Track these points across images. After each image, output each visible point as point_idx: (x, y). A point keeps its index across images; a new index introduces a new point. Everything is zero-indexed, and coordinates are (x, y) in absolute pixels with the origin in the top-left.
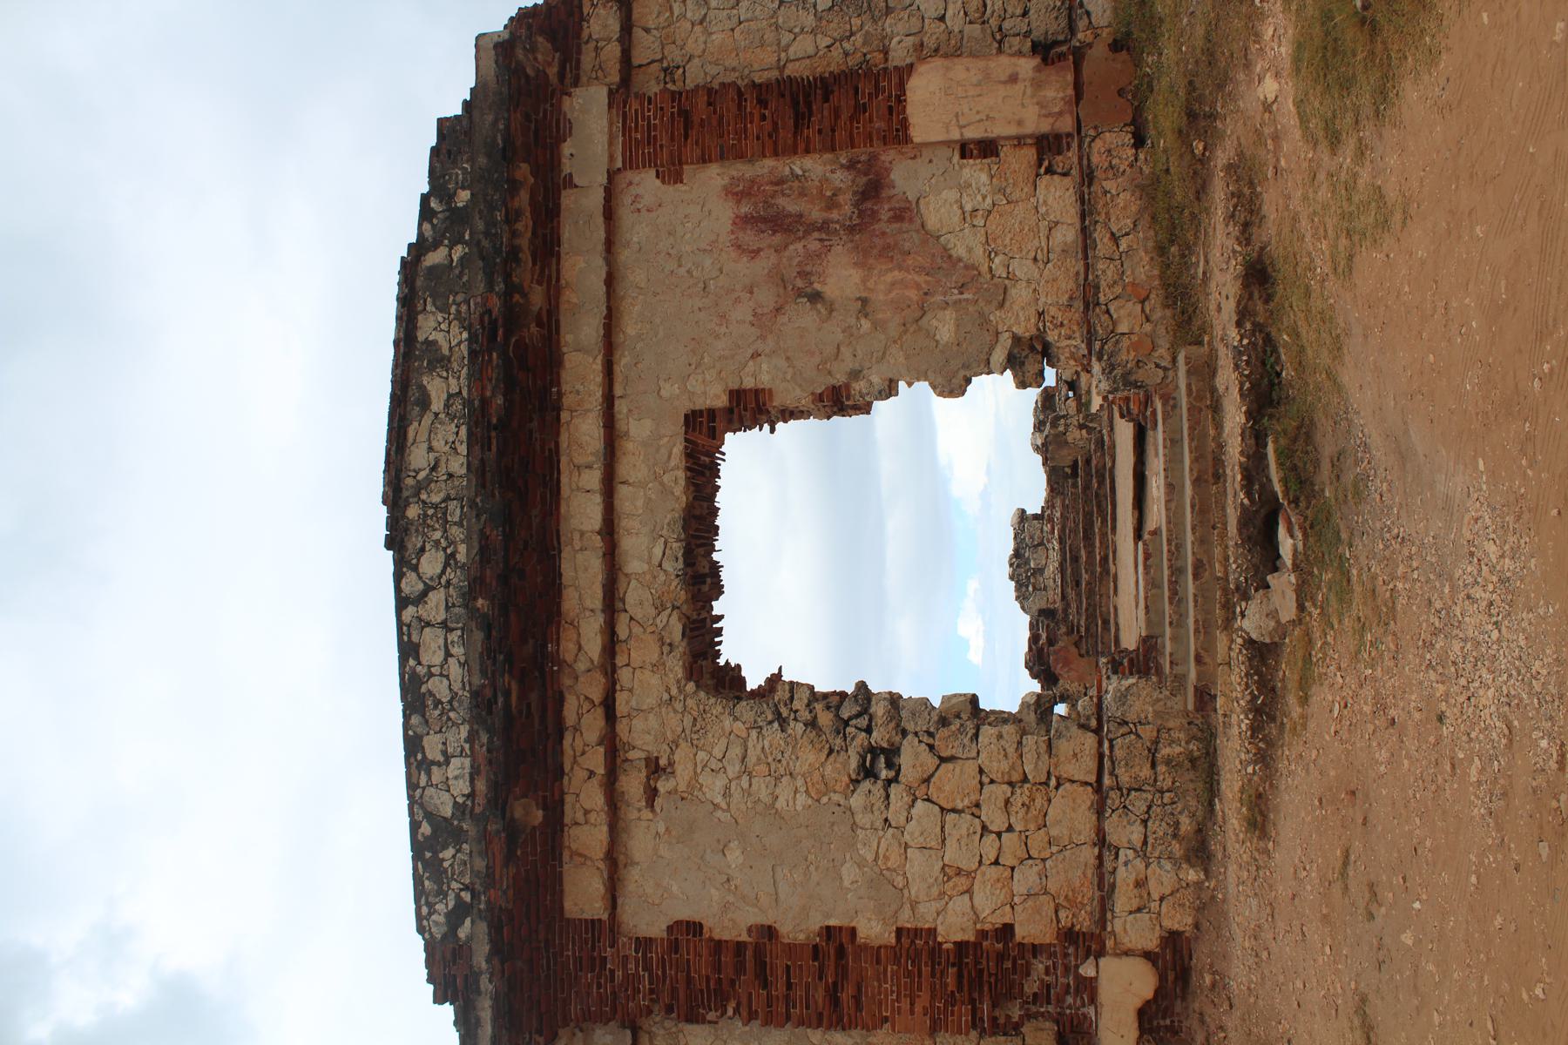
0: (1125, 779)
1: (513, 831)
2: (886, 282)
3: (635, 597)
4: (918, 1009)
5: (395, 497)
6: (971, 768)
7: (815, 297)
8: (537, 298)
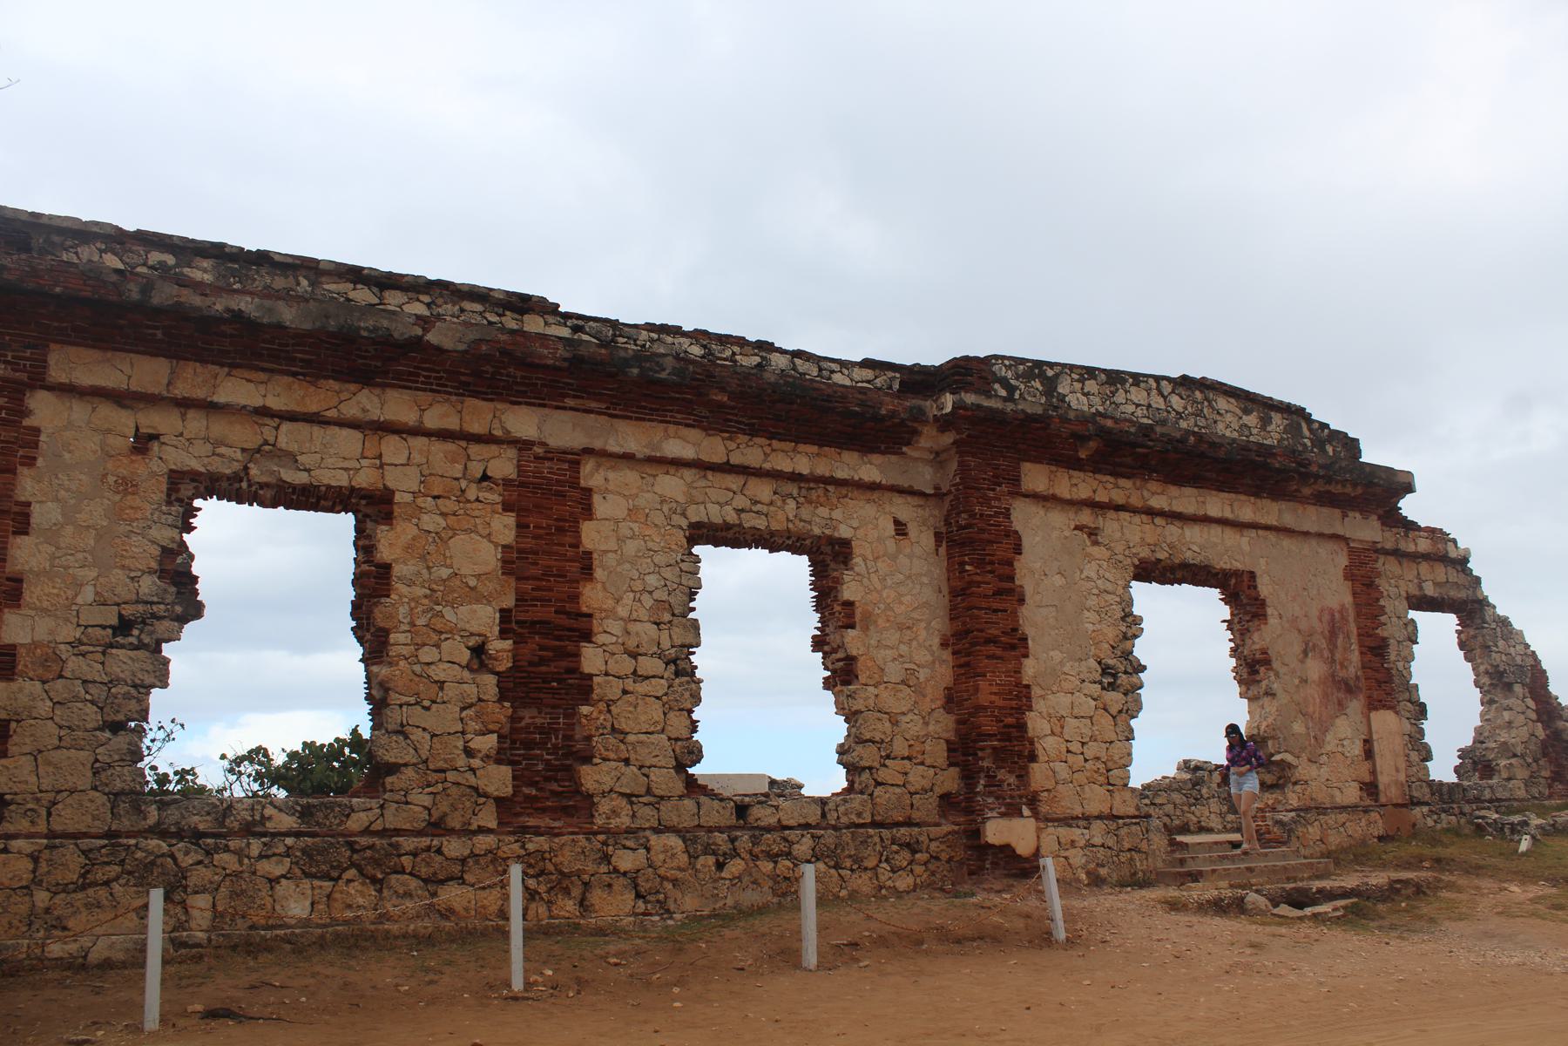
1: (1082, 439)
2: (1313, 693)
3: (1173, 531)
4: (993, 698)
5: (1205, 385)
6: (1113, 737)
7: (1305, 653)
8: (1306, 491)
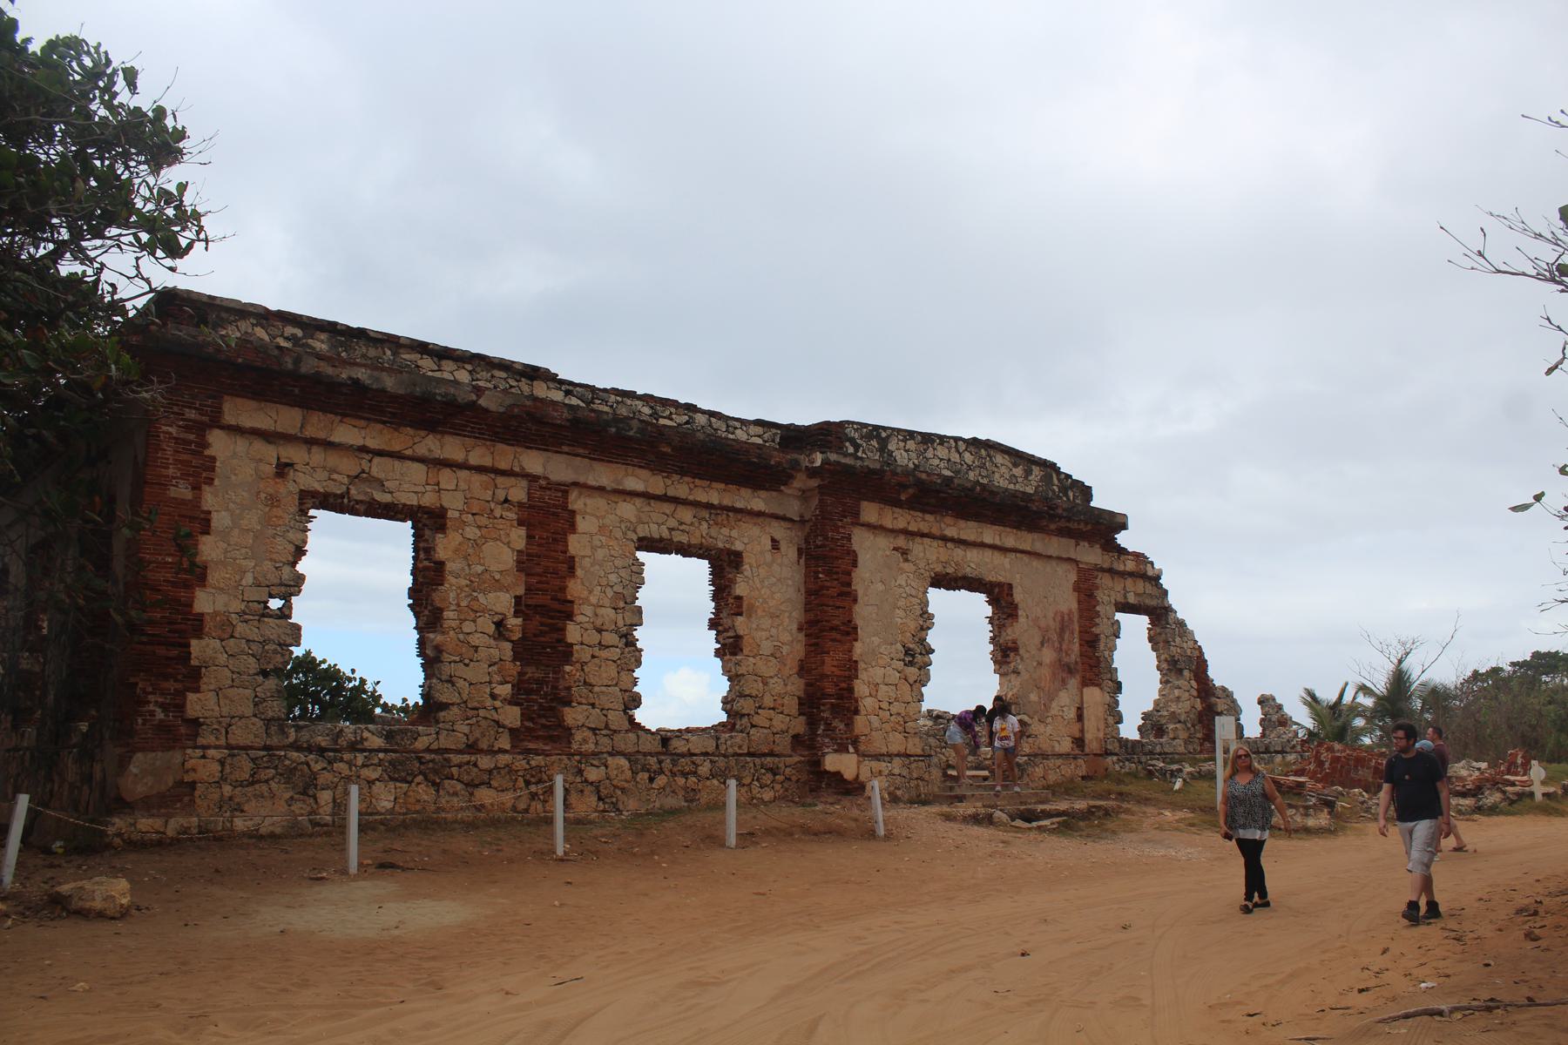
0: (913, 766)
7: (1042, 644)
8: (1053, 527)
